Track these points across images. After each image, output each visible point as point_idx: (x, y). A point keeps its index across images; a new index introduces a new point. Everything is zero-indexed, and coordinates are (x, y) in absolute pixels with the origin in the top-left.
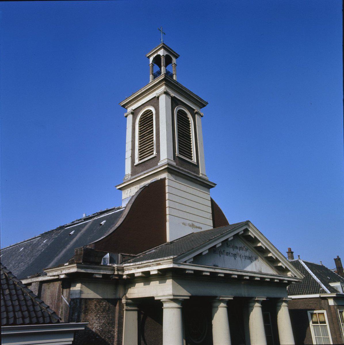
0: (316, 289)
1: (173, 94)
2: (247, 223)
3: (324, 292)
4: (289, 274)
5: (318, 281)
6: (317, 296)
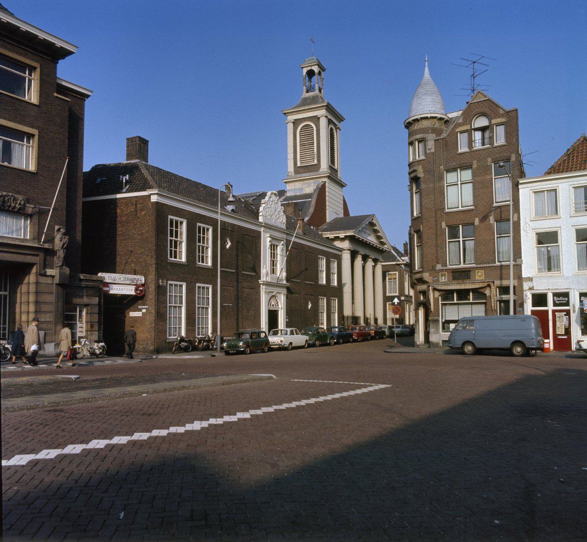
0: (394, 259)
1: (330, 117)
2: (373, 215)
3: (398, 261)
4: (385, 246)
5: (396, 255)
6: (394, 263)
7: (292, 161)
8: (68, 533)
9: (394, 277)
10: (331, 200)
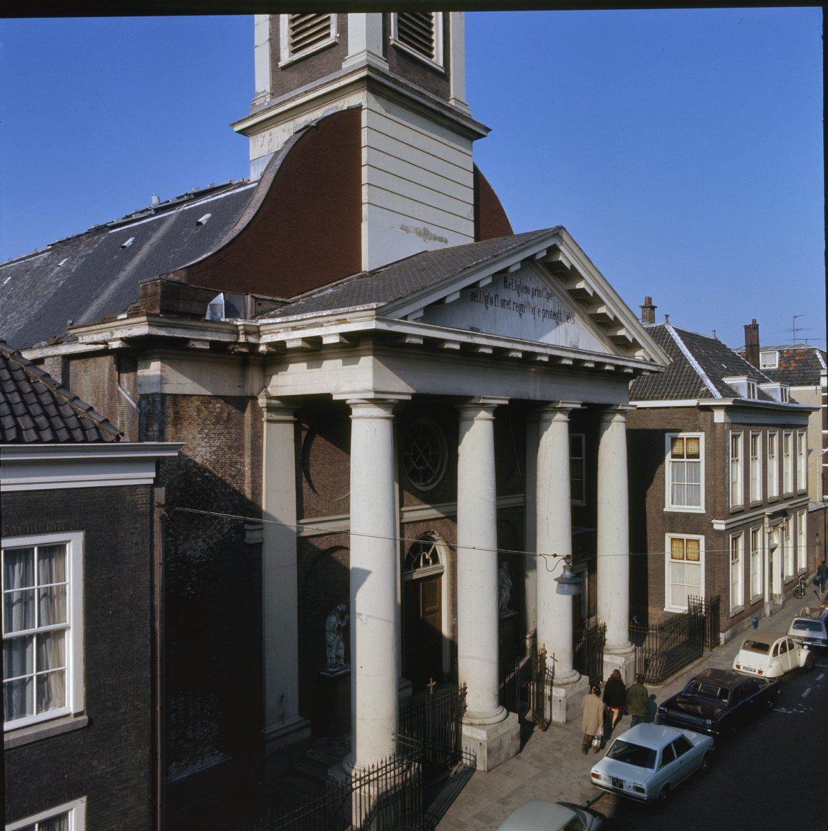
2: (558, 232)
3: (708, 395)
4: (639, 354)
6: (692, 402)
7: (267, 48)
8: (812, 669)
9: (692, 448)
10: (383, 199)
